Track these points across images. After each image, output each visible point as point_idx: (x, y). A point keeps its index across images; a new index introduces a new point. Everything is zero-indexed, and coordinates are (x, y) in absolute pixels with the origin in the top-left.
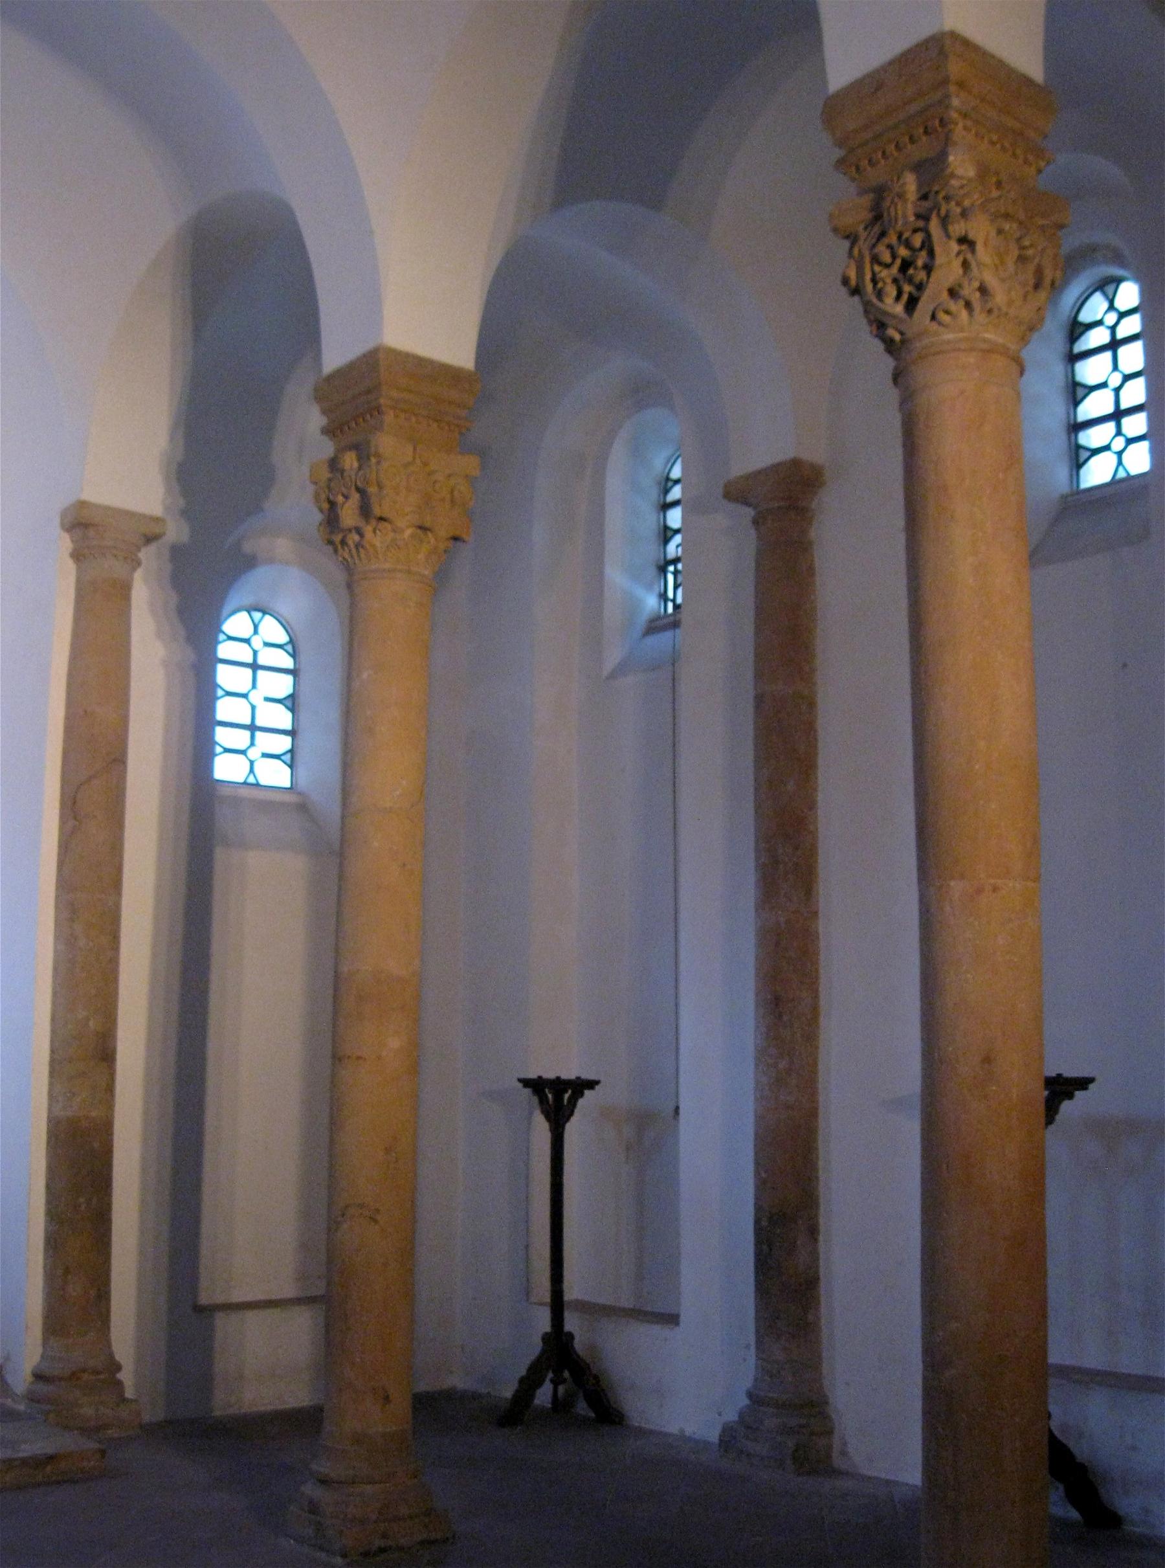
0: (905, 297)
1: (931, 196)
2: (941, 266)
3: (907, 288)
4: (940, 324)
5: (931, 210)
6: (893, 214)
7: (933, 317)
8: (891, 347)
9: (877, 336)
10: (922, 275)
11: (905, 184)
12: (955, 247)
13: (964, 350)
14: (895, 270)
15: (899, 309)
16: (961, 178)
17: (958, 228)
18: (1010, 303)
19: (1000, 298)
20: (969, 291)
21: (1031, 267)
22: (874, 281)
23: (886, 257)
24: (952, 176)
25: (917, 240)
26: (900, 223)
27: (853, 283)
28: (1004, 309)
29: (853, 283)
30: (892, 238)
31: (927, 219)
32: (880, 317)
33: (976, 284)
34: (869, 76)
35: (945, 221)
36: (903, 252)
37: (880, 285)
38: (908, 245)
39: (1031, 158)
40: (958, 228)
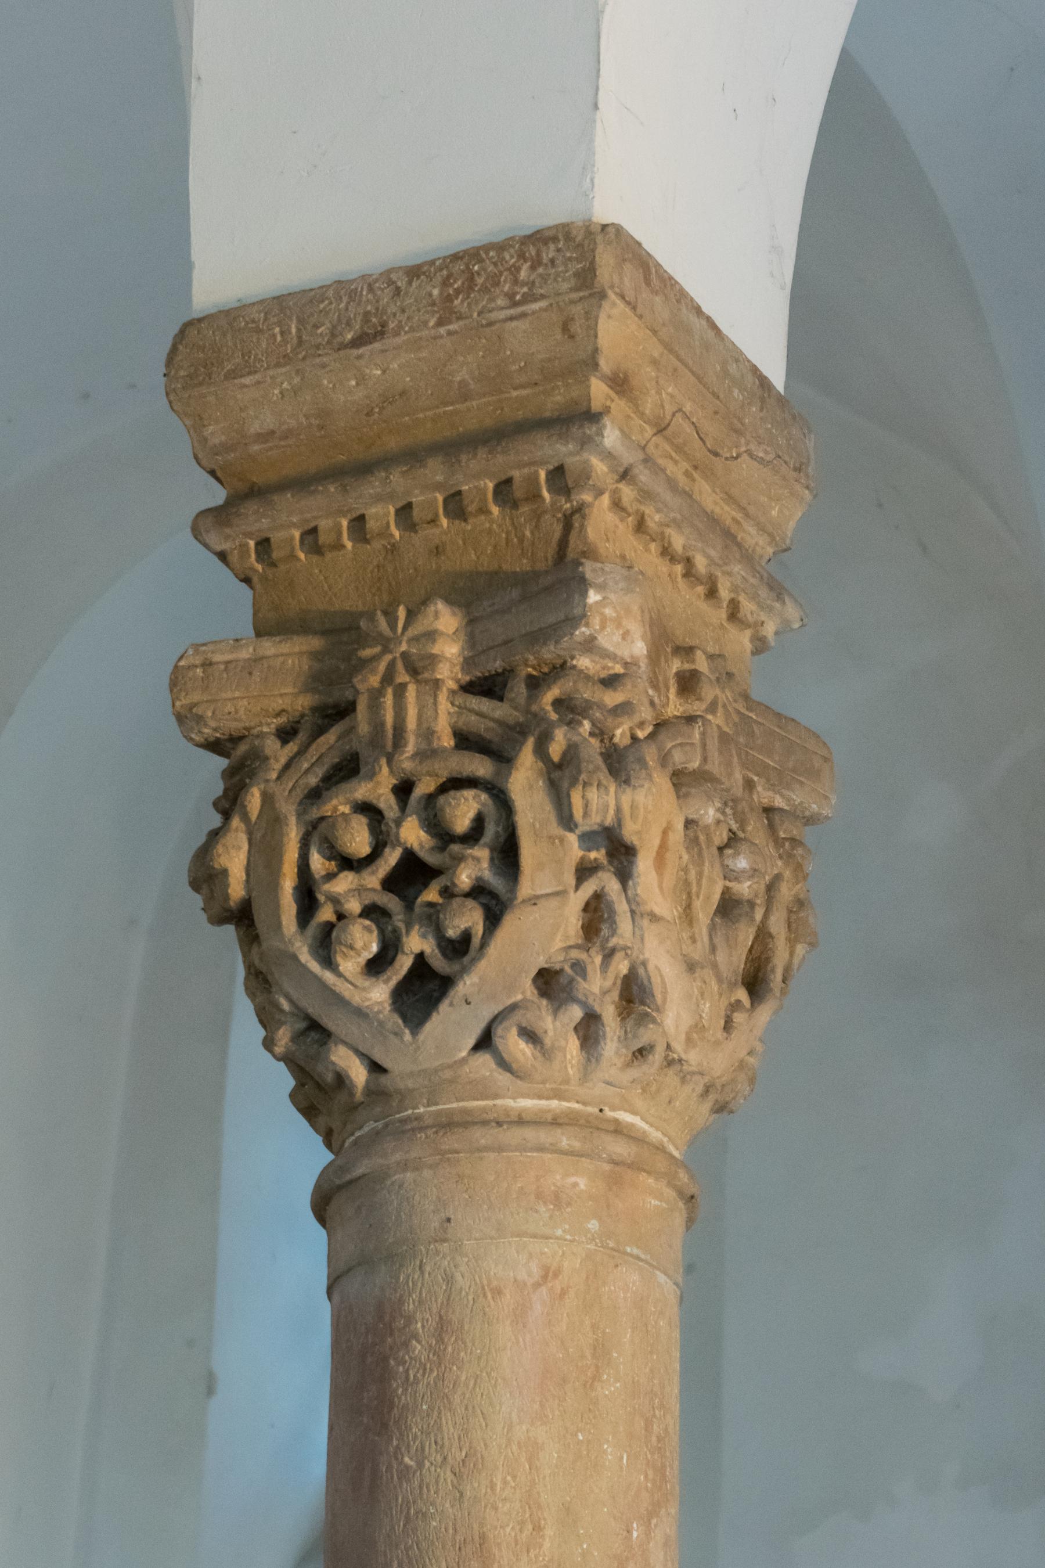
0: (404, 964)
1: (519, 690)
2: (534, 901)
3: (417, 942)
4: (504, 1064)
5: (518, 732)
6: (389, 718)
7: (485, 1042)
8: (318, 1097)
9: (288, 1059)
10: (468, 918)
11: (431, 635)
14: (373, 878)
15: (378, 994)
16: (606, 654)
20: (599, 986)
21: (746, 935)
22: (307, 898)
23: (358, 840)
24: (589, 645)
26: (411, 746)
27: (236, 890)
28: (678, 1047)
29: (236, 890)
30: (379, 787)
31: (502, 757)
32: (315, 1009)
33: (621, 966)
34: (344, 289)
35: (560, 776)
36: (413, 834)
37: (326, 914)
40: (597, 801)
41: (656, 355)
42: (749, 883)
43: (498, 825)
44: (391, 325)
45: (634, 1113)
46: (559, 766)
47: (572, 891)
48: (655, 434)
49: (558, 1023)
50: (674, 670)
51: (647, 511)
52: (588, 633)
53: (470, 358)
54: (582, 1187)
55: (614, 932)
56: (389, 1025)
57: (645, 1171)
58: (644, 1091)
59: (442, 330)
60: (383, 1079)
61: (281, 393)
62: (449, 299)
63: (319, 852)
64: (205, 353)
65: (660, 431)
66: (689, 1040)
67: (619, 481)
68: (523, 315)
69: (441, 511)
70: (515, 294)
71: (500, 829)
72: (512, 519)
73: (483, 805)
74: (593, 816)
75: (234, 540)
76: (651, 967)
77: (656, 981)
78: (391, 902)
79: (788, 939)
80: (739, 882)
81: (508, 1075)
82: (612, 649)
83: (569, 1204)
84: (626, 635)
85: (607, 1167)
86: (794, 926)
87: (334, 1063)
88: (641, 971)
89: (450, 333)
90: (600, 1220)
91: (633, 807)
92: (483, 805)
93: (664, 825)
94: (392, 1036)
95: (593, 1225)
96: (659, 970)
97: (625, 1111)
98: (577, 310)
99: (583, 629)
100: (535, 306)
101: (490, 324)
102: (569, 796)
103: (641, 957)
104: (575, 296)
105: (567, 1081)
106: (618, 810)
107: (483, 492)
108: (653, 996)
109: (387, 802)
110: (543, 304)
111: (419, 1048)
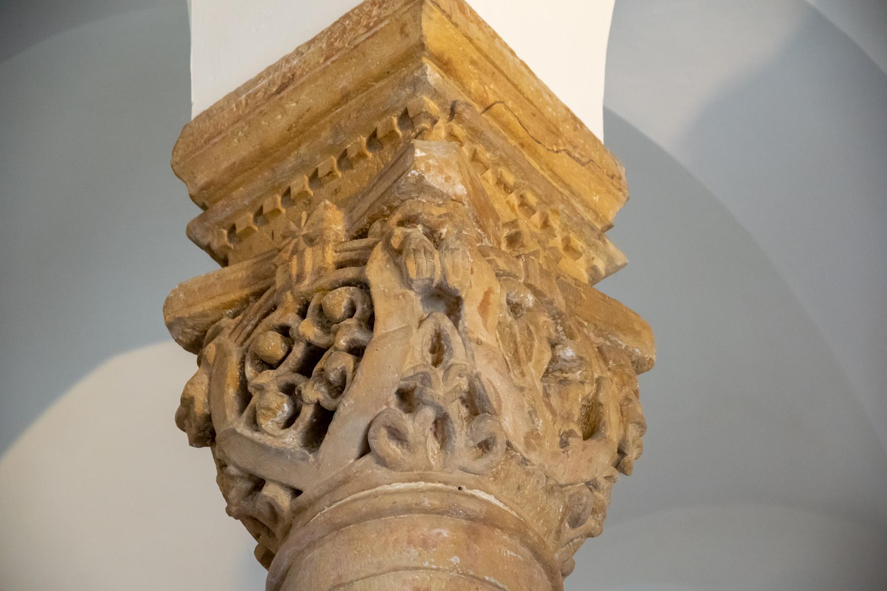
0: (307, 413)
4: (382, 461)
7: (366, 449)
12: (416, 303)
13: (426, 511)
15: (292, 438)
17: (426, 267)
18: (533, 438)
19: (511, 422)
20: (444, 390)
22: (245, 396)
23: (273, 344)
25: (339, 301)
35: (397, 255)
38: (327, 322)
39: (578, 243)
40: (426, 267)
41: (475, 58)
42: (580, 372)
43: (363, 304)
44: (298, 73)
45: (490, 493)
46: (399, 252)
47: (414, 330)
48: (484, 112)
49: (416, 424)
50: (505, 235)
51: (478, 149)
52: (417, 174)
53: (347, 74)
54: (445, 535)
55: (451, 356)
56: (298, 455)
57: (498, 527)
58: (495, 478)
59: (328, 63)
60: (301, 498)
61: (239, 140)
62: (332, 44)
63: (251, 366)
64: (195, 141)
65: (488, 109)
66: (528, 444)
67: (450, 120)
68: (376, 33)
69: (335, 166)
70: (369, 24)
71: (365, 306)
72: (380, 156)
73: (352, 294)
74: (424, 272)
75: (213, 231)
76: (483, 378)
77: (490, 392)
78: (297, 378)
79: (621, 421)
80: (573, 372)
81: (385, 469)
82: (438, 187)
83: (435, 546)
84: (447, 179)
85: (465, 522)
86: (625, 413)
87: (265, 496)
88: (477, 383)
89: (333, 62)
90: (461, 556)
91: (454, 266)
92: (352, 294)
93: (486, 289)
94: (301, 462)
95: (455, 560)
96: (491, 383)
97: (480, 489)
98: (408, 16)
99: (413, 172)
100: (383, 25)
101: (356, 47)
102: (405, 264)
103: (475, 371)
104: (405, 9)
105: (430, 468)
106: (444, 269)
107: (359, 144)
108: (489, 402)
109: (291, 319)
110: (386, 22)
111: (320, 465)
